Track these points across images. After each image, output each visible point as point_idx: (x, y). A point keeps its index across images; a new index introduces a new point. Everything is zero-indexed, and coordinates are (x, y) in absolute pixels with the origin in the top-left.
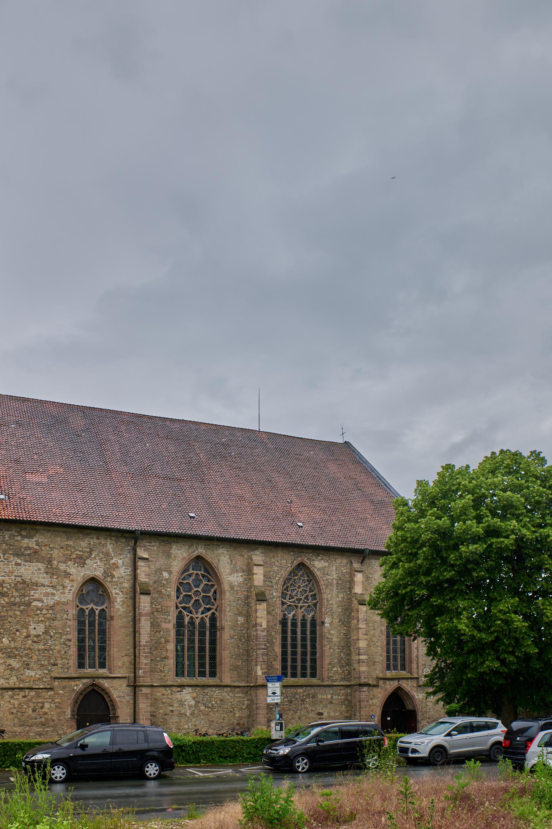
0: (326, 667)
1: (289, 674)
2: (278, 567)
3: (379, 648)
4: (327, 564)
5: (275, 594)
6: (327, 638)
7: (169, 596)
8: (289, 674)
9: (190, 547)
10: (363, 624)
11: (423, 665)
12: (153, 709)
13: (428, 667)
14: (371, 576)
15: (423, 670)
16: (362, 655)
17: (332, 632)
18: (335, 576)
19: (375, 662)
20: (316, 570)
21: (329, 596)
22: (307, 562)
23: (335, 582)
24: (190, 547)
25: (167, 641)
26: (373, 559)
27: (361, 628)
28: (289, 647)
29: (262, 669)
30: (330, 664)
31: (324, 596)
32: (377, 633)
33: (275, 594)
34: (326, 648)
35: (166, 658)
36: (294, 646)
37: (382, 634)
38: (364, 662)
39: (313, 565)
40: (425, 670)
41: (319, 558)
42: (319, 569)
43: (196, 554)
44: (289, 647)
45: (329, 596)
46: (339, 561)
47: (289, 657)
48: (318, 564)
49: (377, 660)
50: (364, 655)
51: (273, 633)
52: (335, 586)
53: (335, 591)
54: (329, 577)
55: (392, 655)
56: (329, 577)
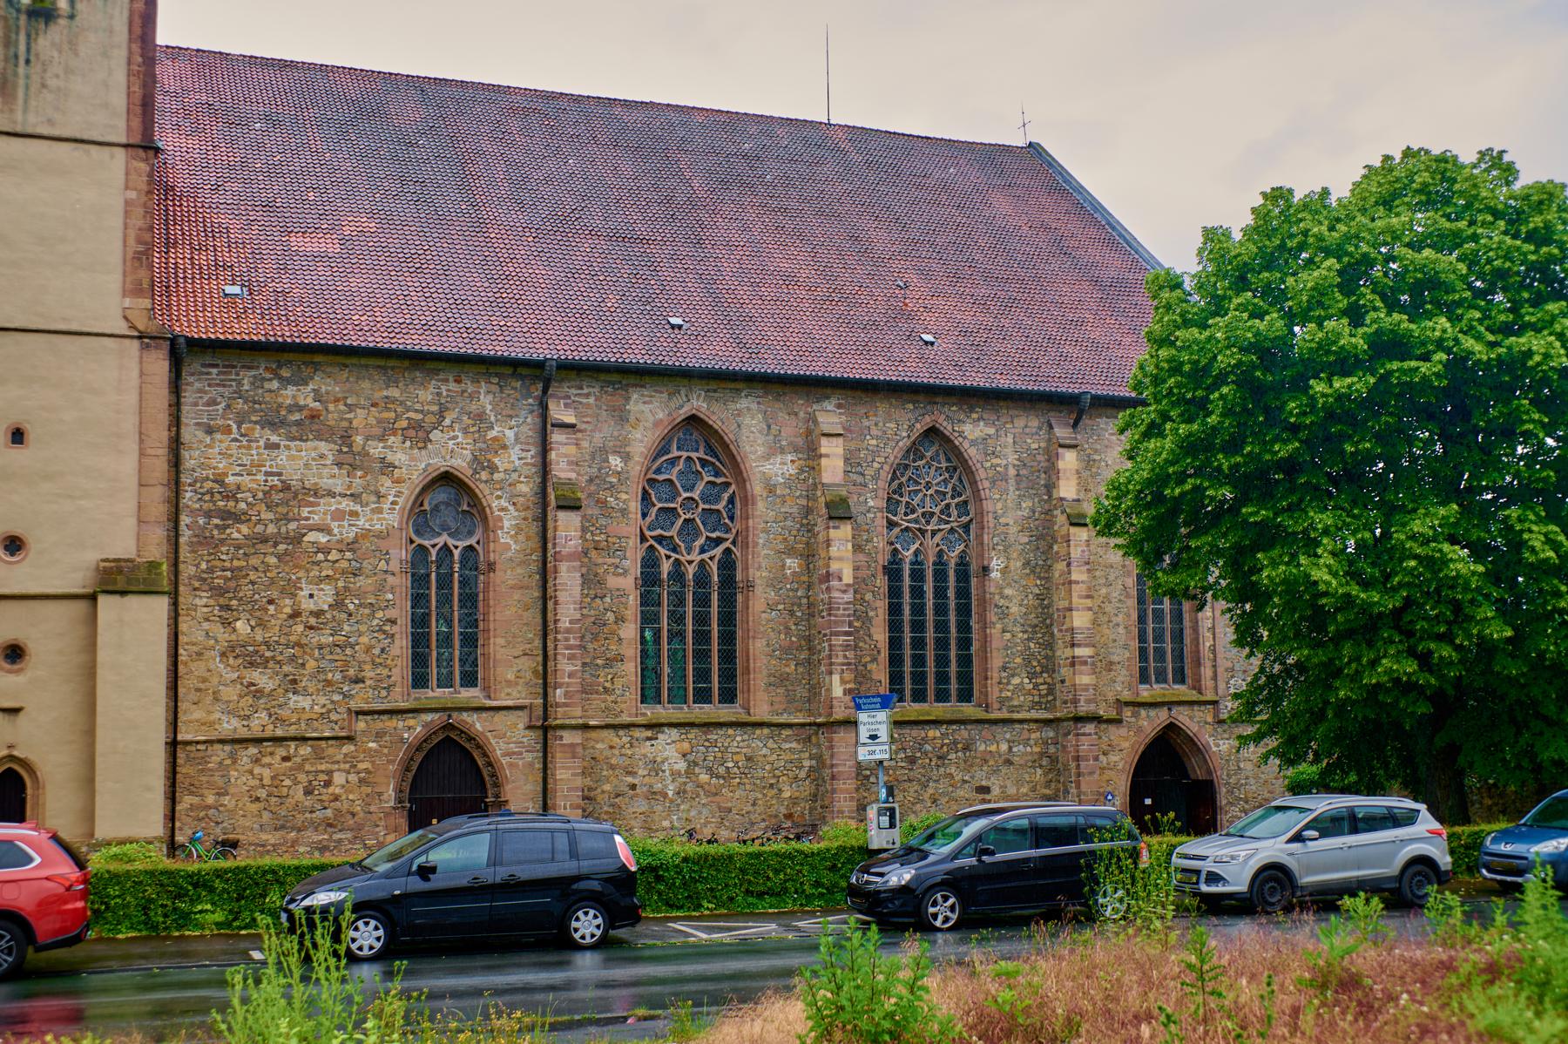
3: (1121, 630)
4: (992, 431)
5: (871, 503)
7: (624, 512)
12: (588, 782)
14: (1097, 457)
17: (1008, 591)
18: (1012, 458)
19: (1111, 663)
20: (966, 444)
21: (999, 505)
22: (946, 427)
25: (620, 619)
26: (1100, 416)
29: (843, 682)
30: (1004, 668)
33: (871, 503)
36: (918, 626)
37: (1128, 596)
38: (1085, 663)
39: (961, 433)
41: (975, 416)
42: (973, 443)
45: (999, 505)
49: (1115, 658)
52: (1012, 482)
53: (1013, 494)
54: (998, 461)
56: (998, 461)
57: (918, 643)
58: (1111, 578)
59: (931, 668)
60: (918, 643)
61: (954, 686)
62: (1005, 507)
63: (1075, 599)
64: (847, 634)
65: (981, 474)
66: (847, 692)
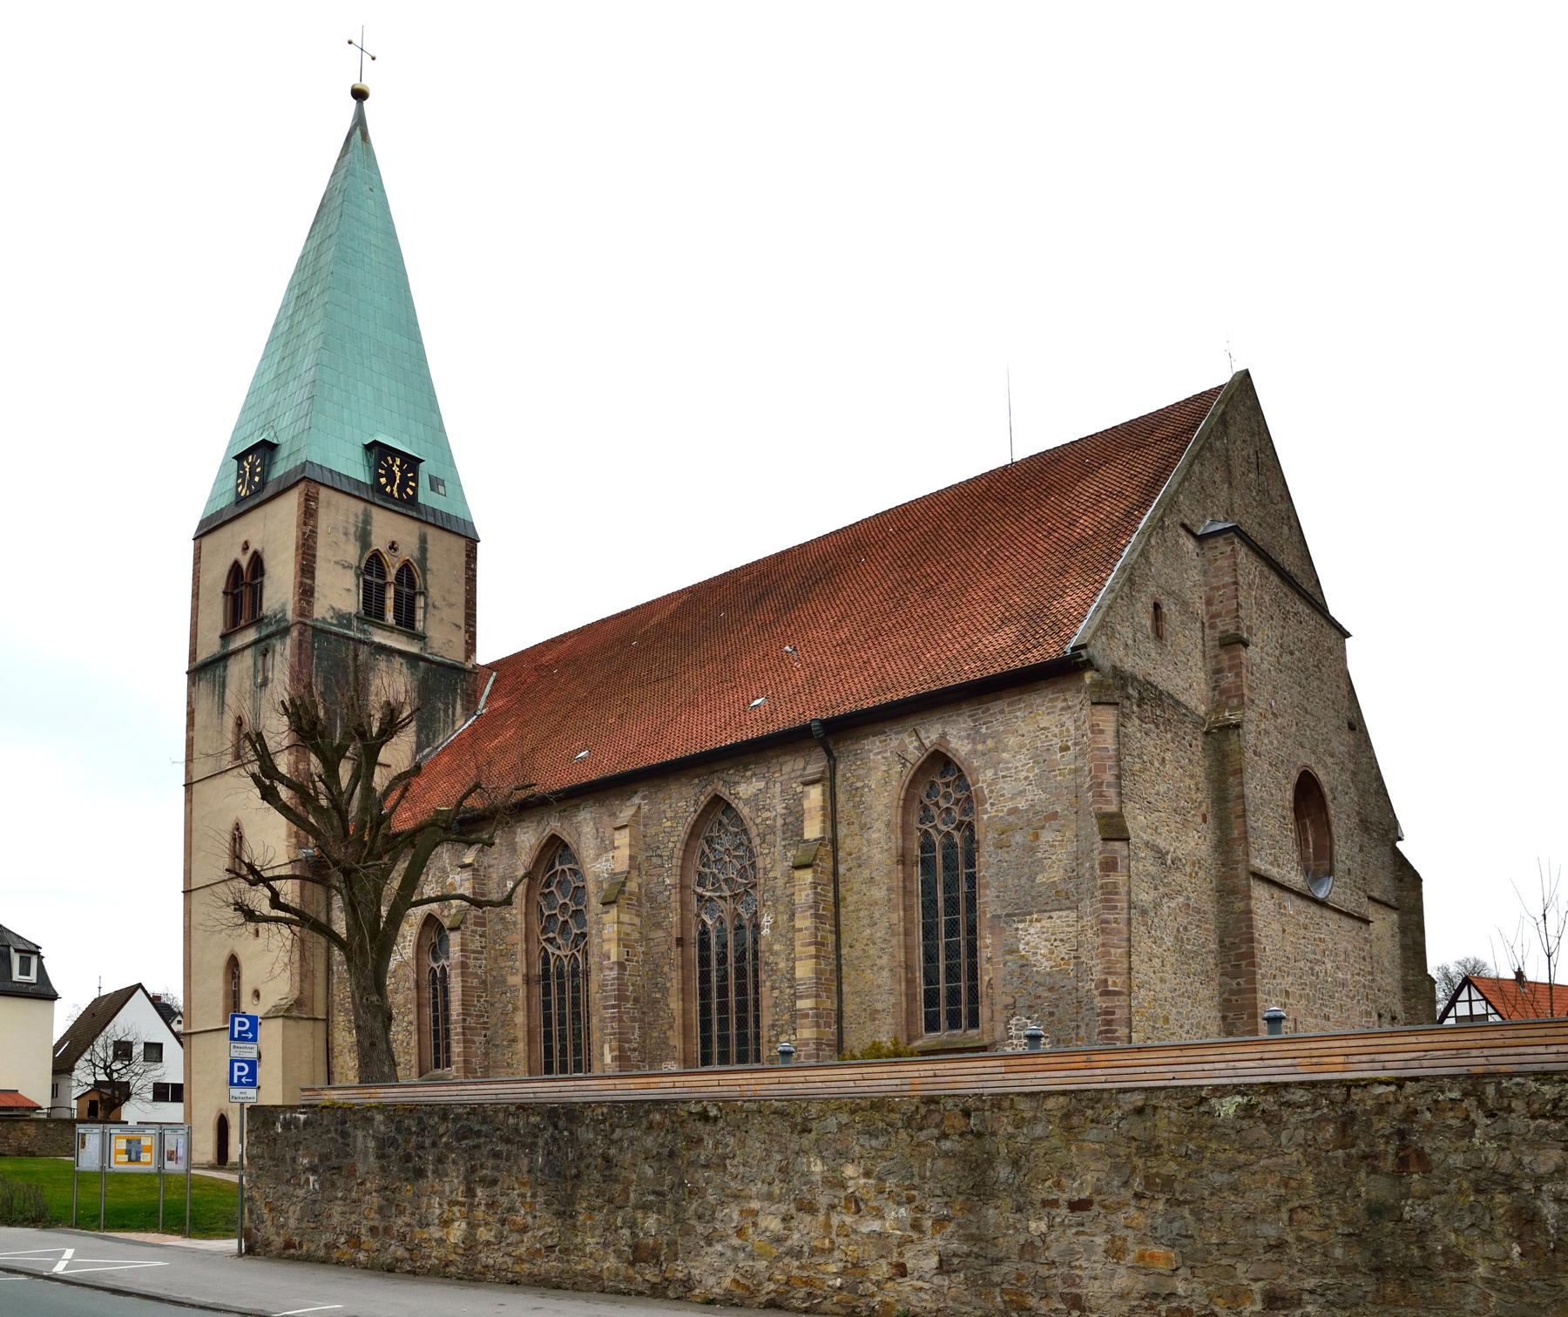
0: (765, 1033)
1: (716, 1056)
2: (672, 819)
3: (885, 974)
4: (762, 785)
5: (668, 881)
6: (767, 964)
7: (515, 923)
8: (716, 1056)
9: (539, 822)
10: (804, 918)
11: (1006, 1007)
12: (1283, 1191)
13: (1024, 1011)
14: (859, 784)
15: (1008, 1022)
16: (801, 997)
17: (777, 947)
18: (780, 809)
19: (877, 1011)
20: (741, 805)
21: (768, 860)
22: (724, 792)
23: (780, 822)
24: (539, 822)
25: (515, 1009)
26: (866, 736)
27: (800, 930)
28: (714, 994)
29: (611, 1050)
30: (773, 1026)
31: (760, 863)
32: (880, 933)
33: (668, 881)
34: (765, 990)
35: (514, 1040)
36: (723, 991)
37: (893, 934)
38: (807, 1016)
39: (736, 796)
40: (1013, 1021)
41: (749, 773)
42: (747, 802)
43: (547, 833)
44: (714, 994)
45: (768, 860)
46: (786, 769)
47: (715, 1017)
48: (746, 789)
49: (879, 1006)
50: (808, 997)
51: (666, 969)
52: (779, 833)
53: (780, 843)
54: (767, 814)
55: (942, 985)
56: (767, 814)
57: (723, 1008)
58: (877, 915)
59: (733, 1030)
60: (723, 1008)
61: (733, 1049)
62: (774, 861)
63: (798, 949)
64: (613, 1007)
65: (753, 832)
66: (614, 1059)
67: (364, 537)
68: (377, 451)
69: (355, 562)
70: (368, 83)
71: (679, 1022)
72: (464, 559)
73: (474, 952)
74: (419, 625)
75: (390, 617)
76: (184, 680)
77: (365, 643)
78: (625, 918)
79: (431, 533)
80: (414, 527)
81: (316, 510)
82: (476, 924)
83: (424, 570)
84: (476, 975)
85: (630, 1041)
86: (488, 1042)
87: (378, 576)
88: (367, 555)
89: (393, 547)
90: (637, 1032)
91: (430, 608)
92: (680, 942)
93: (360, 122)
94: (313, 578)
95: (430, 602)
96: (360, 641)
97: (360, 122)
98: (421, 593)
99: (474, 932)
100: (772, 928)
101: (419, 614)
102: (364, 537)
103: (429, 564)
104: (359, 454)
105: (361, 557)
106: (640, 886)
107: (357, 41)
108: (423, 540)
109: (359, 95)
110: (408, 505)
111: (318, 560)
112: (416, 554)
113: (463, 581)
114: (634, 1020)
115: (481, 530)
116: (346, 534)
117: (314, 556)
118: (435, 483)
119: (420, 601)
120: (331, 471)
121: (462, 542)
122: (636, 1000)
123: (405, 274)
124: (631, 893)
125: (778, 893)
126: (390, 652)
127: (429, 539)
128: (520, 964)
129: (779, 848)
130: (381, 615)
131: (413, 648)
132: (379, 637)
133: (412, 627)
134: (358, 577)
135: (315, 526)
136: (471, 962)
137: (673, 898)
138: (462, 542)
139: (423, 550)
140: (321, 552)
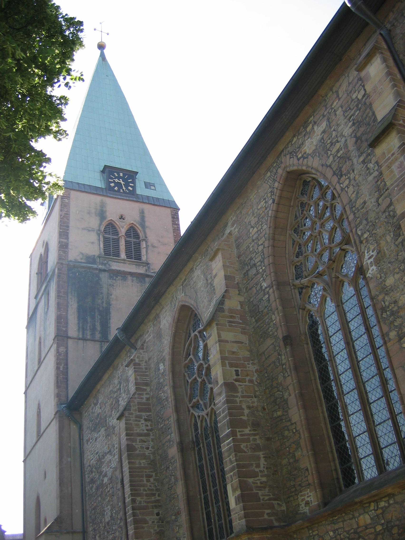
5: (265, 285)
17: (390, 281)
29: (234, 491)
33: (265, 285)
42: (314, 154)
56: (338, 145)
67: (102, 214)
68: (108, 171)
69: (96, 227)
70: (106, 40)
71: (304, 435)
72: (170, 219)
73: (140, 435)
74: (144, 258)
75: (123, 255)
76: (25, 330)
77: (104, 271)
78: (228, 336)
79: (147, 208)
80: (137, 206)
81: (69, 203)
82: (140, 410)
83: (143, 226)
84: (144, 457)
85: (255, 475)
86: (162, 520)
87: (113, 234)
88: (105, 223)
89: (122, 217)
90: (262, 461)
91: (150, 248)
92: (288, 340)
93: (103, 57)
94: (67, 238)
95: (149, 244)
96: (101, 270)
97: (103, 57)
98: (144, 240)
99: (140, 417)
100: (378, 262)
101: (143, 252)
102: (102, 214)
103: (147, 224)
104: (98, 175)
105: (100, 225)
106: (241, 303)
107: (99, 28)
108: (142, 212)
109: (101, 47)
110: (132, 195)
111: (71, 228)
112: (138, 219)
113: (171, 231)
114: (256, 448)
115: (179, 204)
116: (89, 213)
117: (68, 227)
118: (148, 185)
119: (143, 245)
120: (78, 183)
121: (168, 211)
122: (256, 425)
123: (127, 103)
124: (231, 311)
125: (372, 216)
126: (124, 275)
127: (146, 212)
128: (174, 436)
129: (358, 167)
130: (117, 254)
131: (141, 270)
132: (115, 266)
133: (140, 259)
134: (99, 235)
135: (68, 211)
136: (137, 445)
137: (272, 298)
138: (168, 211)
139: (143, 218)
140: (72, 224)
